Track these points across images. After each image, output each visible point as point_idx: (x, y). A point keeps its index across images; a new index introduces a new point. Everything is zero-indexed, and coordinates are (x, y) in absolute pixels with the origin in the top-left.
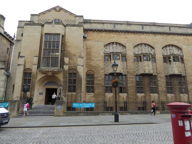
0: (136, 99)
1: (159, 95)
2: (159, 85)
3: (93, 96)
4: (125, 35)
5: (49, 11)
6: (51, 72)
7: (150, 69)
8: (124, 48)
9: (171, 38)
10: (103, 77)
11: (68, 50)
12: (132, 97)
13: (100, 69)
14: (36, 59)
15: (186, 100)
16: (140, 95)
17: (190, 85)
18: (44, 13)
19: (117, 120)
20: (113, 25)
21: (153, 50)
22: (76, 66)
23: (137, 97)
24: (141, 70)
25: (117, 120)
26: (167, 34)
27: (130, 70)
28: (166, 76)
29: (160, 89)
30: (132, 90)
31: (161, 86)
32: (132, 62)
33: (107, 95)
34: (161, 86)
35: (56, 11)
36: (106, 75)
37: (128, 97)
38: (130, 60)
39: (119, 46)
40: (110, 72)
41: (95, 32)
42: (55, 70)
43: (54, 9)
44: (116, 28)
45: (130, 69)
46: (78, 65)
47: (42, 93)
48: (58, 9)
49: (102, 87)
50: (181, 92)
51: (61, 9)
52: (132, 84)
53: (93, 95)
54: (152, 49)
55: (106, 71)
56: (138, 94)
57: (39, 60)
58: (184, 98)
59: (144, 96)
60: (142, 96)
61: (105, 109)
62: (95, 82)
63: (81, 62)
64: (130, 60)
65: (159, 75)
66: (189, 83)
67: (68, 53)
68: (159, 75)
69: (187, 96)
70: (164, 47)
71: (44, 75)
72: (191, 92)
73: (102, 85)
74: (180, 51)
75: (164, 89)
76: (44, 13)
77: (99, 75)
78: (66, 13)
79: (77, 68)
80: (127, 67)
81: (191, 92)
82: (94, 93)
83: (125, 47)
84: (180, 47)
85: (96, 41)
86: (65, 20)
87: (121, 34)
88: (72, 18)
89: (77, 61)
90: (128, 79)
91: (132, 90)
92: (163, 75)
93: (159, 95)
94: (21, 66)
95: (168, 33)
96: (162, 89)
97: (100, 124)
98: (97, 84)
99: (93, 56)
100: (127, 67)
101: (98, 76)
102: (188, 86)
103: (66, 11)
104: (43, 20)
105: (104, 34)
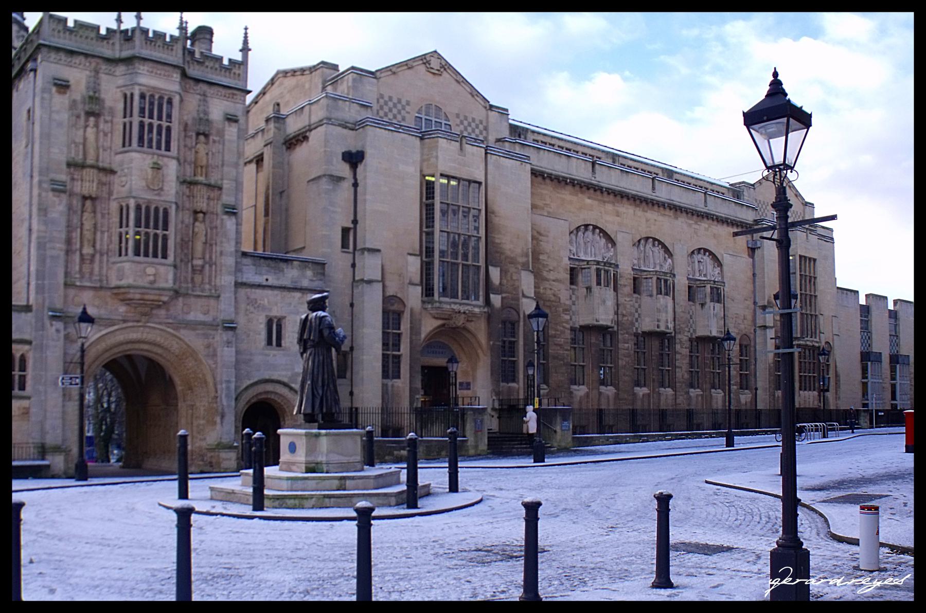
0: (633, 404)
1: (676, 391)
2: (677, 364)
4: (613, 203)
5: (407, 65)
6: (463, 316)
8: (610, 245)
10: (568, 335)
11: (497, 241)
12: (626, 396)
13: (561, 309)
14: (414, 266)
18: (392, 70)
19: (730, 443)
21: (669, 261)
22: (518, 299)
23: (634, 394)
24: (647, 320)
25: (730, 443)
27: (626, 318)
28: (691, 340)
30: (626, 378)
31: (681, 367)
32: (629, 295)
33: (574, 392)
34: (681, 367)
35: (429, 70)
36: (573, 329)
37: (617, 396)
38: (625, 286)
40: (582, 323)
42: (666, 341)
43: (424, 60)
44: (598, 179)
46: (524, 296)
48: (435, 64)
49: (564, 368)
50: (713, 387)
51: (446, 66)
52: (627, 359)
53: (546, 391)
54: (667, 256)
55: (574, 319)
56: (637, 389)
57: (427, 269)
59: (649, 395)
60: (643, 395)
62: (550, 351)
63: (527, 282)
64: (625, 286)
67: (497, 252)
68: (678, 336)
69: (723, 394)
70: (693, 252)
71: (440, 322)
73: (565, 361)
74: (718, 270)
77: (558, 327)
79: (518, 305)
80: (618, 309)
82: (548, 386)
83: (614, 244)
84: (719, 257)
85: (550, 215)
86: (458, 116)
87: (606, 198)
88: (479, 113)
89: (519, 280)
90: (620, 345)
91: (626, 378)
92: (683, 337)
93: (676, 391)
94: (375, 284)
96: (683, 376)
97: (287, 523)
98: (555, 358)
99: (544, 266)
100: (618, 309)
101: (558, 331)
102: (193, 319)
103: (461, 80)
104: (390, 98)
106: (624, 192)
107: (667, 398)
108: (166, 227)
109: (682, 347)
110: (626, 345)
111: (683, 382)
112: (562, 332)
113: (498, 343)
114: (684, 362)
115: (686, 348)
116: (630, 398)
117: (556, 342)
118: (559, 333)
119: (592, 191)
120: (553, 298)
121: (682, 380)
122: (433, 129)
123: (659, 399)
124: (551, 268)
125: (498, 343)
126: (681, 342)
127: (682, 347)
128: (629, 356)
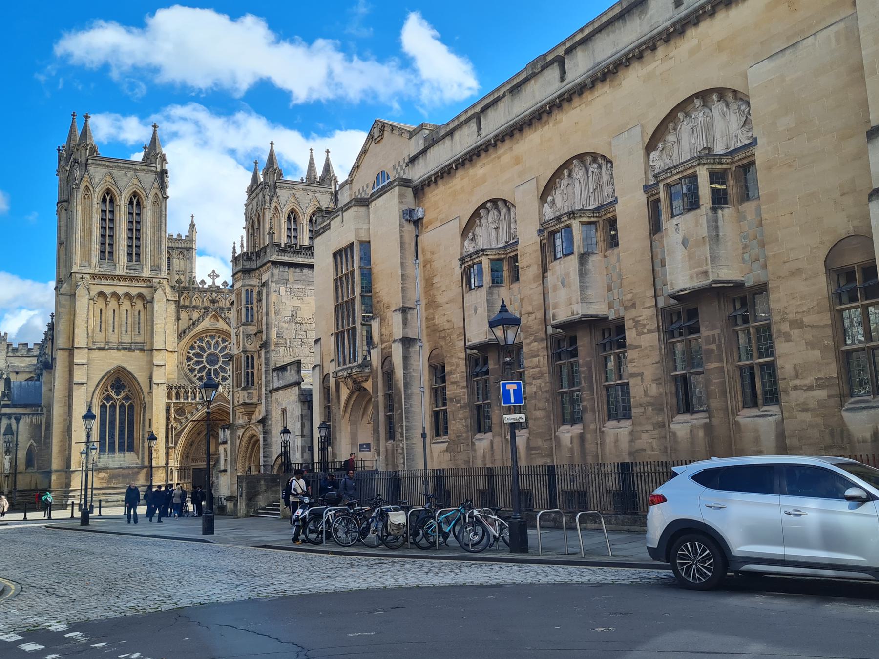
3: (447, 450)
7: (574, 299)
9: (692, 52)
15: (769, 438)
16: (568, 433)
17: (788, 338)
20: (553, 73)
25: (209, 529)
26: (667, 41)
29: (637, 391)
31: (642, 374)
34: (642, 374)
38: (529, 266)
39: (718, 107)
41: (599, 86)
45: (529, 314)
47: (368, 445)
49: (462, 412)
52: (539, 381)
58: (756, 431)
61: (637, 528)
65: (633, 313)
66: (785, 327)
72: (796, 388)
75: (654, 390)
76: (358, 167)
78: (363, 166)
81: (796, 388)
95: (667, 29)
96: (645, 392)
105: (430, 195)
106: (516, 123)
107: (616, 441)
108: (252, 367)
109: (639, 334)
110: (536, 360)
111: (650, 404)
112: (458, 365)
113: (713, 366)
114: (648, 361)
115: (649, 332)
116: (546, 445)
117: (453, 380)
118: (454, 367)
119: (483, 155)
120: (447, 326)
121: (645, 400)
122: (121, 270)
123: (603, 444)
124: (444, 289)
125: (713, 366)
126: (637, 323)
127: (639, 334)
128: (541, 375)
